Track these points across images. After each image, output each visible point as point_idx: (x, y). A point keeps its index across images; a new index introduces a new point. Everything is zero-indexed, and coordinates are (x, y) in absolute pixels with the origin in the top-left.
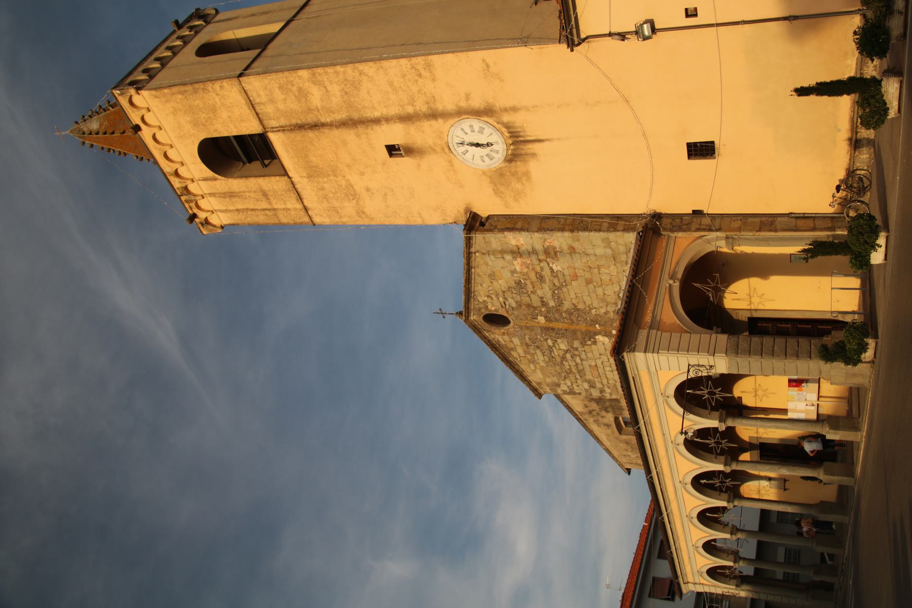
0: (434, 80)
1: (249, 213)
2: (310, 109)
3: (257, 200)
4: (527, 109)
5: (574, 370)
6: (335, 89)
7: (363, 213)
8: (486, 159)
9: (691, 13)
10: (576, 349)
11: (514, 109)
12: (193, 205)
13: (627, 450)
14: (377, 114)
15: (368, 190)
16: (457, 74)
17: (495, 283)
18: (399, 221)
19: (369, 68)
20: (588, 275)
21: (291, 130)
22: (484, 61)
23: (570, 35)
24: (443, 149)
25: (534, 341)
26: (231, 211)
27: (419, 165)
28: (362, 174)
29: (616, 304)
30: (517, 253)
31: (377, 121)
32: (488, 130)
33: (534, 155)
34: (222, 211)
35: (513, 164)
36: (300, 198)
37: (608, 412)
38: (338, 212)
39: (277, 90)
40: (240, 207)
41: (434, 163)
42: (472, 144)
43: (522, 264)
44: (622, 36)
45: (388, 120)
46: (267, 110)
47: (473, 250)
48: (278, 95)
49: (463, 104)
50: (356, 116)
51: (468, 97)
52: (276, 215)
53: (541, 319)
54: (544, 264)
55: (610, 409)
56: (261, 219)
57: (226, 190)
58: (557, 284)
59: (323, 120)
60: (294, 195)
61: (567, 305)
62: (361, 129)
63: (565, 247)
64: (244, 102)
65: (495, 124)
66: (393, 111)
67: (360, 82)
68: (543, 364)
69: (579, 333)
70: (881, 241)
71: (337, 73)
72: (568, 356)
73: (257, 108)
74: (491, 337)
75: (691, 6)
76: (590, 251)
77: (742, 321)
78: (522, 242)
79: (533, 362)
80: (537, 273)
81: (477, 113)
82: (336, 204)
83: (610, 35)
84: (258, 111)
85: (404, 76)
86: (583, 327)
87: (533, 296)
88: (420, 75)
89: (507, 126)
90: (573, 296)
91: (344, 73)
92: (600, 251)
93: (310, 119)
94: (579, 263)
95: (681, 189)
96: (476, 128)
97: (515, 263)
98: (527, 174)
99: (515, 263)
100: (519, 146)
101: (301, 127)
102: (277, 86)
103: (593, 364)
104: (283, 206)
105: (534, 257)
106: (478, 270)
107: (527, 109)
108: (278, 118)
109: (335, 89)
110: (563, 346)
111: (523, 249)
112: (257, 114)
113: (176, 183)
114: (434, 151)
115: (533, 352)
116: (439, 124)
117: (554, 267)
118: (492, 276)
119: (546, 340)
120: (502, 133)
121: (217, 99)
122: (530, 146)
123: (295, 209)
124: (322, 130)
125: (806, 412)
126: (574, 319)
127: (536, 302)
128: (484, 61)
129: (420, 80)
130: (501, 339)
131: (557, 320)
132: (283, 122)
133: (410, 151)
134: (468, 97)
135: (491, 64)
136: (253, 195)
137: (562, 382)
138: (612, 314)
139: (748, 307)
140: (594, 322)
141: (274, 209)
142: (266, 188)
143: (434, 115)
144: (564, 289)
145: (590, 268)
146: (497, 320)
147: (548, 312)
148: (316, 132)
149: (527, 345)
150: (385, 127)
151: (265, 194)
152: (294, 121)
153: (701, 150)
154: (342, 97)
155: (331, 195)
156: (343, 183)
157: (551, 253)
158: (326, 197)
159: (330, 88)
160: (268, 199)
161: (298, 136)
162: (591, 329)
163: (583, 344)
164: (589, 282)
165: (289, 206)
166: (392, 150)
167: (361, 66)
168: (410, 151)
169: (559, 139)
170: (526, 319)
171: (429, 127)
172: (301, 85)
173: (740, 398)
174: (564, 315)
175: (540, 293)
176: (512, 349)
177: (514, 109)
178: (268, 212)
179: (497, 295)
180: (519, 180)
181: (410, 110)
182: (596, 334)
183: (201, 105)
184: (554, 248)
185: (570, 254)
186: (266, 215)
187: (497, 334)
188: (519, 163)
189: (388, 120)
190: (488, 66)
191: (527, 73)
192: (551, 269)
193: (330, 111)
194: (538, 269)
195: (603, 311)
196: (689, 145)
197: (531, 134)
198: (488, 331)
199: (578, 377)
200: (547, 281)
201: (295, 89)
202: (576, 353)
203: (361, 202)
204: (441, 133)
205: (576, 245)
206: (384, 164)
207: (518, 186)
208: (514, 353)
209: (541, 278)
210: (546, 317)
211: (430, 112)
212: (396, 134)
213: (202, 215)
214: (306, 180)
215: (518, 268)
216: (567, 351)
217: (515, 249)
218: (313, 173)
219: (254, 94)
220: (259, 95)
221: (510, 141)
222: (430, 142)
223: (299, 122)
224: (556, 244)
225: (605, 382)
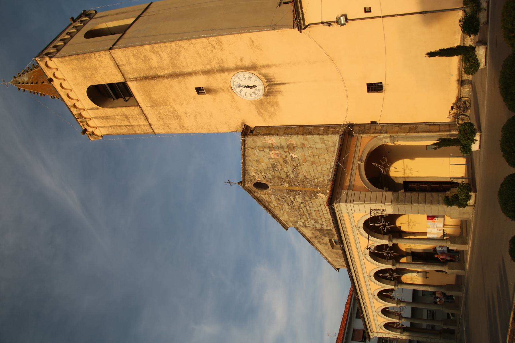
0: (222, 50)
1: (118, 128)
2: (151, 68)
3: (122, 121)
4: (275, 66)
5: (306, 213)
7: (183, 126)
8: (253, 94)
9: (367, 10)
10: (307, 202)
11: (268, 66)
13: (337, 258)
14: (190, 70)
15: (186, 113)
16: (236, 47)
17: (260, 165)
19: (184, 44)
20: (312, 160)
21: (141, 80)
22: (250, 39)
23: (299, 23)
24: (228, 89)
26: (107, 127)
27: (215, 99)
28: (182, 104)
29: (329, 175)
30: (271, 148)
31: (190, 74)
32: (254, 78)
34: (102, 127)
35: (269, 97)
36: (147, 119)
39: (132, 57)
40: (112, 124)
41: (223, 97)
42: (245, 86)
43: (275, 154)
44: (329, 24)
45: (196, 73)
46: (126, 68)
47: (246, 146)
48: (133, 60)
49: (239, 64)
50: (178, 71)
51: (242, 59)
52: (133, 129)
53: (287, 185)
54: (287, 154)
55: (326, 235)
57: (104, 115)
58: (295, 165)
59: (159, 74)
60: (143, 117)
61: (301, 177)
62: (181, 79)
63: (299, 144)
64: (113, 64)
65: (258, 75)
66: (199, 68)
67: (180, 52)
68: (288, 210)
70: (477, 137)
71: (166, 47)
72: (302, 205)
73: (121, 67)
75: (367, 6)
76: (313, 146)
77: (400, 184)
80: (283, 159)
81: (247, 69)
82: (168, 122)
84: (121, 69)
86: (310, 189)
87: (281, 172)
88: (214, 48)
89: (265, 76)
90: (304, 171)
92: (319, 146)
93: (152, 73)
94: (307, 153)
95: (363, 110)
96: (247, 77)
98: (276, 103)
100: (271, 87)
101: (146, 78)
102: (132, 54)
103: (317, 210)
104: (137, 124)
105: (281, 150)
106: (250, 158)
107: (275, 66)
108: (133, 73)
110: (299, 200)
111: (275, 145)
112: (121, 71)
113: (75, 111)
114: (223, 90)
115: (282, 203)
116: (225, 75)
117: (293, 156)
118: (258, 161)
119: (290, 197)
120: (262, 80)
121: (97, 63)
122: (278, 87)
124: (158, 79)
125: (437, 234)
127: (283, 175)
128: (250, 39)
129: (214, 50)
130: (264, 197)
131: (295, 185)
132: (136, 75)
133: (209, 91)
135: (255, 41)
136: (119, 117)
138: (326, 181)
139: (404, 176)
140: (317, 186)
141: (132, 126)
142: (127, 114)
143: (222, 70)
144: (299, 168)
145: (314, 155)
147: (290, 181)
149: (279, 200)
150: (194, 77)
151: (126, 117)
152: (142, 75)
153: (375, 88)
154: (170, 60)
155: (164, 117)
156: (171, 110)
157: (291, 147)
159: (162, 56)
161: (144, 83)
162: (315, 190)
163: (311, 198)
165: (140, 123)
166: (199, 90)
167: (180, 43)
168: (209, 91)
169: (294, 83)
170: (278, 185)
172: (146, 54)
173: (400, 227)
175: (285, 170)
176: (270, 202)
177: (268, 66)
178: (128, 127)
179: (261, 172)
180: (272, 106)
181: (209, 67)
183: (88, 66)
184: (293, 144)
185: (302, 148)
187: (262, 194)
188: (272, 97)
189: (196, 73)
190: (253, 42)
191: (276, 45)
193: (163, 69)
195: (321, 179)
196: (368, 85)
197: (278, 80)
198: (256, 193)
199: (308, 217)
200: (290, 163)
201: (142, 56)
202: (307, 204)
203: (182, 120)
204: (227, 80)
205: (305, 142)
207: (272, 110)
208: (271, 205)
209: (286, 162)
210: (289, 184)
211: (220, 68)
212: (201, 81)
213: (90, 130)
215: (273, 156)
216: (301, 203)
217: (271, 145)
218: (154, 104)
219: (119, 60)
220: (121, 60)
221: (266, 84)
222: (221, 86)
223: (145, 75)
224: (294, 142)
225: (323, 219)
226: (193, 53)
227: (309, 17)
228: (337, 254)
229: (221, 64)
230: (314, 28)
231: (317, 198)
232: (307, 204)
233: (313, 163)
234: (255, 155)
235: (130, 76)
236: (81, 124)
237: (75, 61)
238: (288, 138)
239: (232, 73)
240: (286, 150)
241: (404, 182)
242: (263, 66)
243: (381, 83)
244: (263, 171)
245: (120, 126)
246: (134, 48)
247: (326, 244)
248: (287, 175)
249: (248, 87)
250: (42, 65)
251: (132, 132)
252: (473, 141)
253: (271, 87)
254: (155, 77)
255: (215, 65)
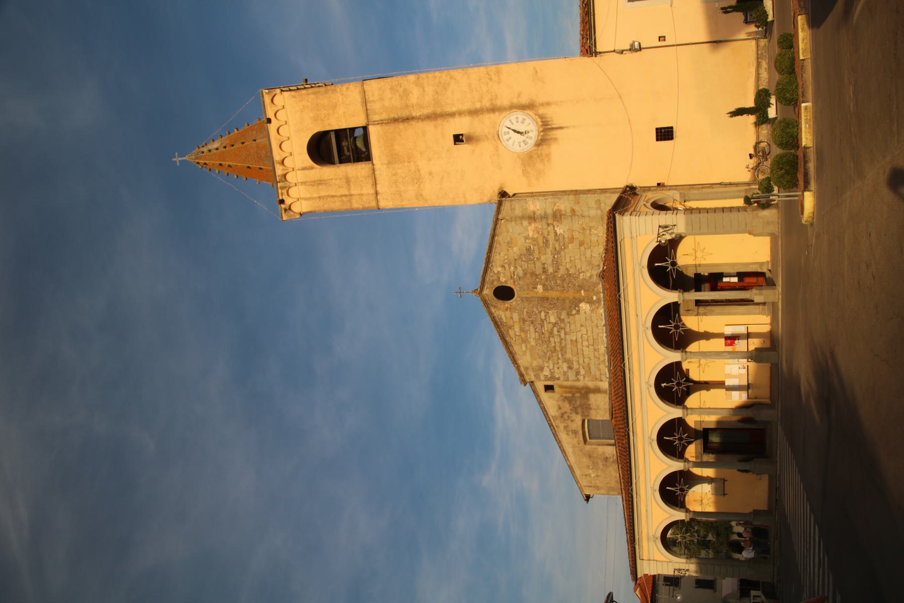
0: (499, 83)
2: (407, 106)
3: (340, 187)
5: (558, 348)
6: (430, 90)
7: (421, 195)
8: (522, 144)
9: (662, 38)
10: (563, 320)
11: (548, 104)
12: (285, 191)
13: (588, 467)
14: (454, 109)
15: (430, 174)
16: (516, 79)
17: (511, 251)
18: (446, 202)
19: (457, 74)
20: (581, 238)
21: (388, 123)
22: (535, 68)
23: (589, 48)
25: (529, 314)
26: (313, 198)
27: (474, 151)
28: (430, 160)
29: (599, 266)
30: (532, 218)
31: (452, 115)
32: (528, 121)
33: (556, 139)
34: (305, 199)
36: (375, 183)
37: (577, 413)
38: (401, 196)
40: (323, 194)
41: (484, 149)
42: (515, 131)
43: (536, 230)
44: (622, 52)
45: (460, 113)
46: (375, 106)
48: (388, 94)
49: (515, 101)
50: (439, 111)
51: (519, 95)
52: (350, 201)
53: (540, 288)
54: (551, 228)
55: (579, 410)
56: (336, 205)
57: (317, 178)
58: (558, 248)
59: (414, 114)
60: (370, 181)
61: (562, 271)
62: (439, 121)
63: (569, 210)
66: (466, 106)
68: (533, 343)
69: (567, 301)
70: (773, 100)
71: (435, 77)
72: (555, 329)
73: (368, 105)
74: (497, 313)
76: (586, 213)
77: (690, 278)
78: (538, 207)
79: (525, 341)
80: (544, 237)
81: (523, 107)
83: (614, 51)
84: (368, 107)
85: (480, 80)
86: (570, 294)
87: (537, 263)
88: (491, 79)
90: (568, 260)
91: (440, 77)
92: (593, 213)
93: (405, 113)
94: (577, 225)
95: (648, 166)
96: (520, 120)
97: (530, 228)
98: (548, 156)
99: (530, 228)
101: (396, 120)
103: (574, 339)
104: (359, 192)
105: (544, 221)
109: (430, 90)
111: (538, 213)
112: (367, 110)
113: (279, 171)
114: (487, 137)
115: (527, 328)
117: (558, 232)
118: (510, 244)
119: (540, 312)
122: (554, 132)
123: (368, 194)
125: (739, 376)
126: (565, 285)
127: (539, 270)
128: (535, 68)
130: (503, 317)
131: (552, 289)
132: (384, 116)
133: (470, 139)
134: (519, 95)
136: (338, 182)
137: (546, 364)
138: (595, 277)
139: (694, 263)
140: (581, 287)
141: (351, 195)
142: (350, 175)
143: (493, 109)
144: (562, 253)
146: (504, 293)
147: (547, 279)
148: (406, 125)
149: (524, 321)
152: (392, 116)
156: (413, 168)
157: (558, 216)
158: (396, 182)
159: (426, 89)
160: (349, 185)
161: (391, 128)
162: (577, 295)
163: (569, 314)
164: (581, 244)
165: (364, 191)
166: (458, 139)
167: (452, 73)
168: (470, 139)
170: (528, 289)
171: (487, 118)
173: (688, 370)
174: (558, 282)
175: (543, 258)
176: (510, 328)
177: (548, 104)
178: (344, 198)
181: (478, 105)
182: (580, 301)
184: (560, 211)
186: (342, 201)
187: (502, 310)
189: (460, 113)
190: (536, 72)
191: (562, 78)
192: (556, 232)
193: (421, 107)
194: (546, 233)
195: (588, 274)
198: (495, 307)
201: (401, 89)
205: (576, 208)
206: (448, 151)
208: (511, 332)
209: (546, 242)
210: (544, 285)
212: (461, 125)
213: (288, 201)
214: (385, 166)
215: (531, 234)
216: (555, 324)
217: (532, 214)
218: (393, 159)
220: (373, 95)
224: (562, 207)
225: (581, 361)
226: (461, 86)
227: (603, 42)
228: (590, 457)
229: (494, 102)
230: (605, 56)
231: (578, 312)
232: (562, 325)
233: (581, 244)
234: (508, 231)
235: (376, 118)
236: (280, 191)
237: (313, 96)
238: (556, 200)
239: (504, 114)
240: (550, 221)
241: (696, 275)
242: (542, 105)
243: (672, 128)
244: (513, 262)
245: (333, 196)
246: (394, 78)
247: (575, 432)
248: (544, 268)
249: (518, 132)
250: (267, 99)
251: (346, 206)
252: (768, 105)
253: (547, 129)
254: (407, 119)
255: (487, 104)
